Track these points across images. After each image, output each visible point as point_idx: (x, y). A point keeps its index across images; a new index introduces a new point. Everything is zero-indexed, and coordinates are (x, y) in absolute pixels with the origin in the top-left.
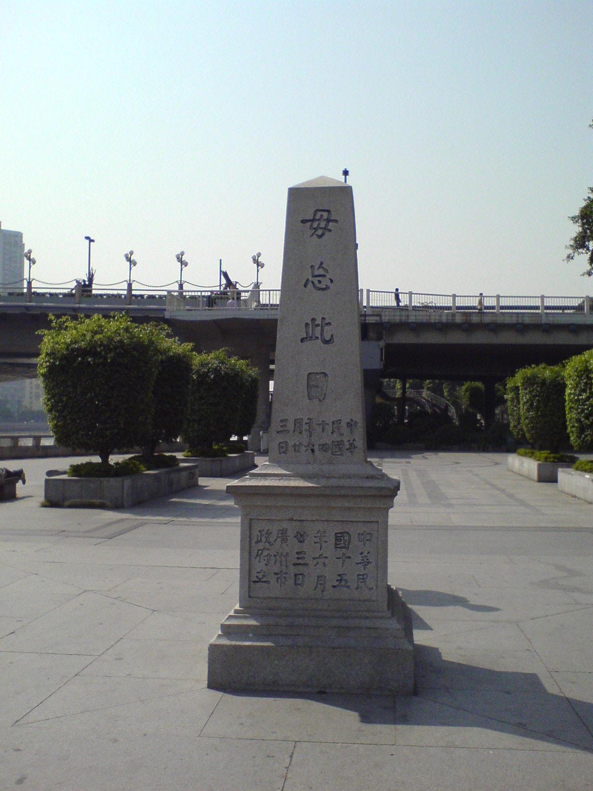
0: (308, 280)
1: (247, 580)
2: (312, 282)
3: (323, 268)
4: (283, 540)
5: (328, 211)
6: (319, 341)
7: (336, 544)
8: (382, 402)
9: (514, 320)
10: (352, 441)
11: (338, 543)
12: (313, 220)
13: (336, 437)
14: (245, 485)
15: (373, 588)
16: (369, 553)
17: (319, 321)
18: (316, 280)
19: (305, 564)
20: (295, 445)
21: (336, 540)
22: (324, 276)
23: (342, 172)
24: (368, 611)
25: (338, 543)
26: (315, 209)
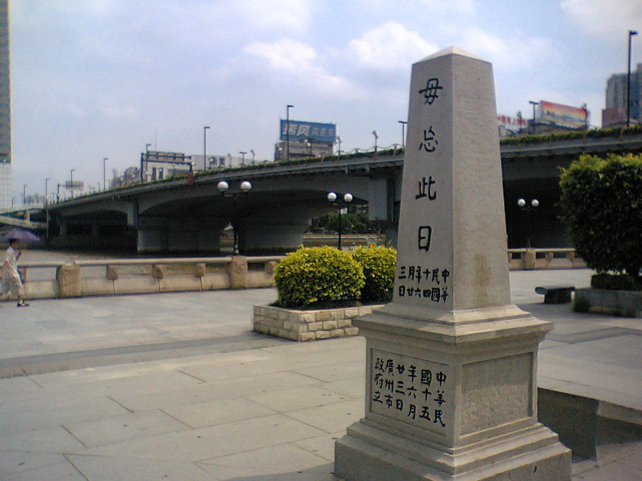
0: (422, 144)
1: (369, 398)
2: (425, 145)
3: (432, 132)
4: (390, 369)
5: (437, 80)
6: (427, 198)
7: (422, 380)
8: (572, 298)
9: (562, 153)
10: (445, 289)
11: (424, 379)
12: (426, 90)
13: (434, 285)
14: (365, 320)
15: (407, 446)
16: (443, 392)
17: (427, 181)
18: (426, 143)
19: (403, 393)
20: (409, 290)
21: (423, 376)
22: (431, 139)
23: (449, 45)
24: (439, 443)
25: (424, 379)
26: (428, 80)
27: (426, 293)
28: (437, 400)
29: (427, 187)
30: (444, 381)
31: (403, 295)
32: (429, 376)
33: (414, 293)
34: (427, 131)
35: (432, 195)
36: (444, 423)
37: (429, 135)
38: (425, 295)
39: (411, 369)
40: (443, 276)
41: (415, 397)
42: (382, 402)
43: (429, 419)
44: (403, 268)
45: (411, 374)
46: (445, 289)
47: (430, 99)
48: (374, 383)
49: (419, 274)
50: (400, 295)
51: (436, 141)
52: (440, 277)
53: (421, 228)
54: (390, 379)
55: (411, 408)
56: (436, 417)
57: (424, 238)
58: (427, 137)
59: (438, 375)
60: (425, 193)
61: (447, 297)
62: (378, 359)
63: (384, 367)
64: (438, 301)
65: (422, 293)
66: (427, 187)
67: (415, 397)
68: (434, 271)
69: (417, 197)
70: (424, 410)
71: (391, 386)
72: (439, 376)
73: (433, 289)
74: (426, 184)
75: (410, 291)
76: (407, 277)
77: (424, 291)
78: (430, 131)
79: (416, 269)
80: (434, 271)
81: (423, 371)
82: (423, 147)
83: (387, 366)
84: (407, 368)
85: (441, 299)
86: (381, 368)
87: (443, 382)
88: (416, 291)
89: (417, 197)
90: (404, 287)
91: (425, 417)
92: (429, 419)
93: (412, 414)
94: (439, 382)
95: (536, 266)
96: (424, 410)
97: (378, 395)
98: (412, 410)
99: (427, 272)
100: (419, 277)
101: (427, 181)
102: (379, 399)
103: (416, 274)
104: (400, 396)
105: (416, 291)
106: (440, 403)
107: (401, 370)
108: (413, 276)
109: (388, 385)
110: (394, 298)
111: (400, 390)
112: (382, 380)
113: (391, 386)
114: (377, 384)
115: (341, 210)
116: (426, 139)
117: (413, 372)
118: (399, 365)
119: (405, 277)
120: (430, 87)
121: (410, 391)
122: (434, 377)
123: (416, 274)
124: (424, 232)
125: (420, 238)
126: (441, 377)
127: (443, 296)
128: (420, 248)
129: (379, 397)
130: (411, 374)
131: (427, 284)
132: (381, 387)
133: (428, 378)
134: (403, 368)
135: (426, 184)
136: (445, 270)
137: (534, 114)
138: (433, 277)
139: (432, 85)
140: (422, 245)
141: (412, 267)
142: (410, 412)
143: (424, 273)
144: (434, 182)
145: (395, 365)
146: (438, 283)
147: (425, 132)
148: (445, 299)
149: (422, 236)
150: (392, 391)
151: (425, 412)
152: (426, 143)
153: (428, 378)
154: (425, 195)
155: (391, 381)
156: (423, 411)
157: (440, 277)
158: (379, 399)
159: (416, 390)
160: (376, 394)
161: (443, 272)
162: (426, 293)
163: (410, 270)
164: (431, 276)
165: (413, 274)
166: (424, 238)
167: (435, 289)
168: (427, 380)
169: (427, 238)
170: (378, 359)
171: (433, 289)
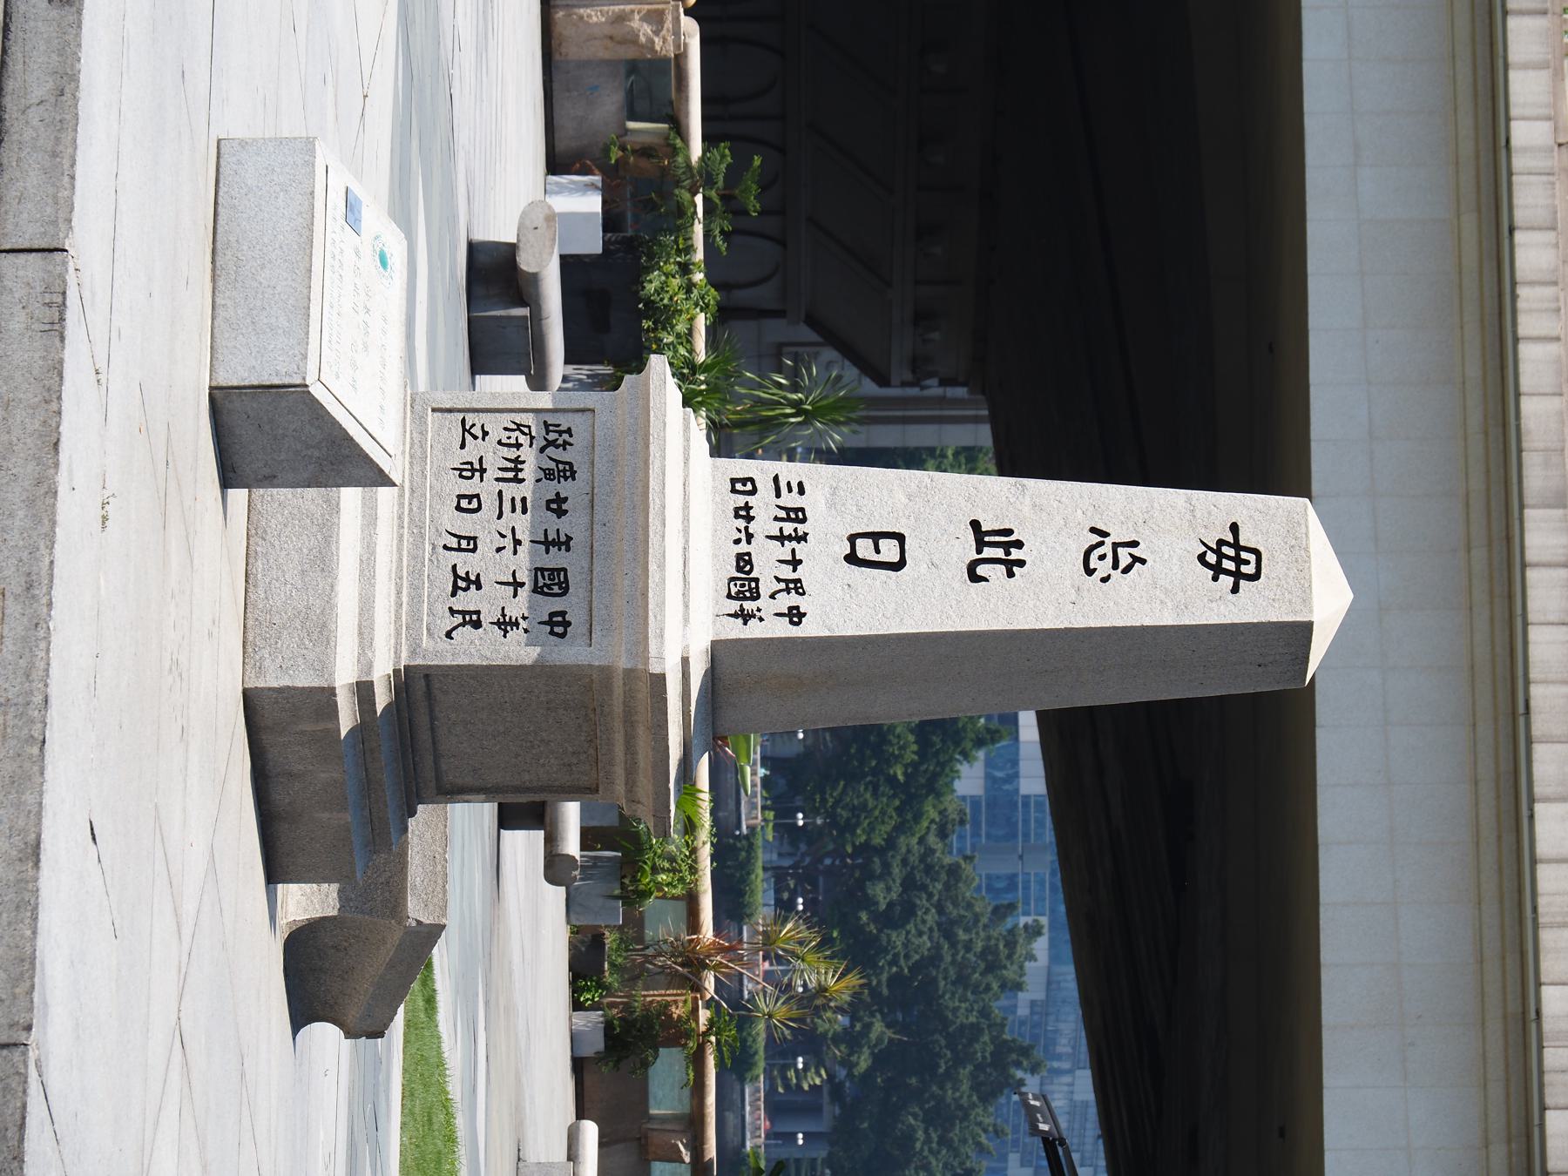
0: (1105, 534)
7: (542, 570)
13: (766, 587)
17: (1015, 554)
18: (1107, 549)
20: (747, 507)
21: (552, 570)
22: (1115, 566)
26: (1261, 549)
27: (743, 561)
28: (504, 615)
29: (999, 553)
30: (552, 633)
31: (734, 491)
32: (556, 589)
33: (741, 523)
34: (1135, 551)
35: (981, 570)
36: (454, 634)
37: (1124, 556)
38: (739, 557)
39: (563, 539)
40: (791, 609)
41: (499, 550)
42: (463, 446)
43: (454, 594)
44: (802, 491)
45: (550, 539)
46: (757, 614)
47: (1211, 558)
48: (506, 420)
49: (790, 538)
50: (734, 481)
51: (1109, 576)
52: (786, 601)
53: (900, 538)
54: (529, 472)
55: (468, 539)
56: (464, 613)
57: (878, 551)
58: (1120, 550)
59: (563, 614)
60: (986, 549)
61: (740, 621)
62: (569, 431)
63: (550, 451)
64: (729, 596)
65: (743, 547)
66: (999, 553)
67: (499, 550)
68: (799, 581)
69: (975, 525)
70: (473, 578)
71: (511, 475)
72: (560, 619)
73: (756, 580)
74: (1008, 553)
75: (744, 513)
76: (781, 502)
77: (749, 554)
78: (1137, 559)
79: (801, 528)
80: (799, 581)
81: (565, 570)
82: (1096, 539)
83: (558, 462)
84: (565, 525)
85: (734, 606)
86: (551, 443)
87: (548, 628)
88: (746, 528)
89: (975, 525)
90: (754, 492)
91: (455, 583)
92: (454, 594)
93: (453, 543)
94: (546, 618)
95: (531, 415)
96: (473, 578)
97: (477, 431)
98: (464, 544)
99: (795, 563)
100: (781, 538)
101: (1015, 554)
102: (468, 437)
103: (788, 528)
104: (489, 503)
105: (746, 528)
106: (498, 624)
107: (554, 506)
108: (782, 520)
109: (513, 465)
110: (723, 462)
111: (507, 506)
112: (518, 446)
113: (511, 475)
114: (506, 429)
115: (653, 1111)
116: (1115, 546)
117: (557, 543)
118: (566, 499)
119: (778, 495)
120: (1244, 555)
121: (510, 536)
122: (557, 604)
123: (788, 528)
124: (889, 551)
125: (876, 537)
126: (558, 624)
127: (742, 609)
128: (852, 539)
129: (475, 437)
130: (550, 539)
131: (768, 562)
132: (500, 443)
133: (549, 587)
134: (561, 513)
135: (1008, 553)
136: (805, 614)
137: (1549, 894)
138: (787, 581)
139: (1247, 562)
140: (859, 542)
141: (804, 514)
142: (460, 537)
143: (793, 551)
144: (1011, 574)
145: (565, 488)
146: (772, 596)
147: (1134, 544)
148: (735, 615)
149: (881, 542)
150: (498, 480)
151: (467, 579)
152: (1107, 549)
153: (549, 587)
154: (979, 551)
155: (521, 476)
156: (467, 573)
157: (786, 601)
158: (468, 437)
159: (515, 552)
160: (478, 426)
161: (797, 608)
162: (743, 561)
163: (796, 510)
164: (786, 572)
165: (788, 519)
166: (878, 551)
167: (757, 587)
168: (545, 585)
169: (876, 558)
170: (569, 431)
171: (756, 580)
